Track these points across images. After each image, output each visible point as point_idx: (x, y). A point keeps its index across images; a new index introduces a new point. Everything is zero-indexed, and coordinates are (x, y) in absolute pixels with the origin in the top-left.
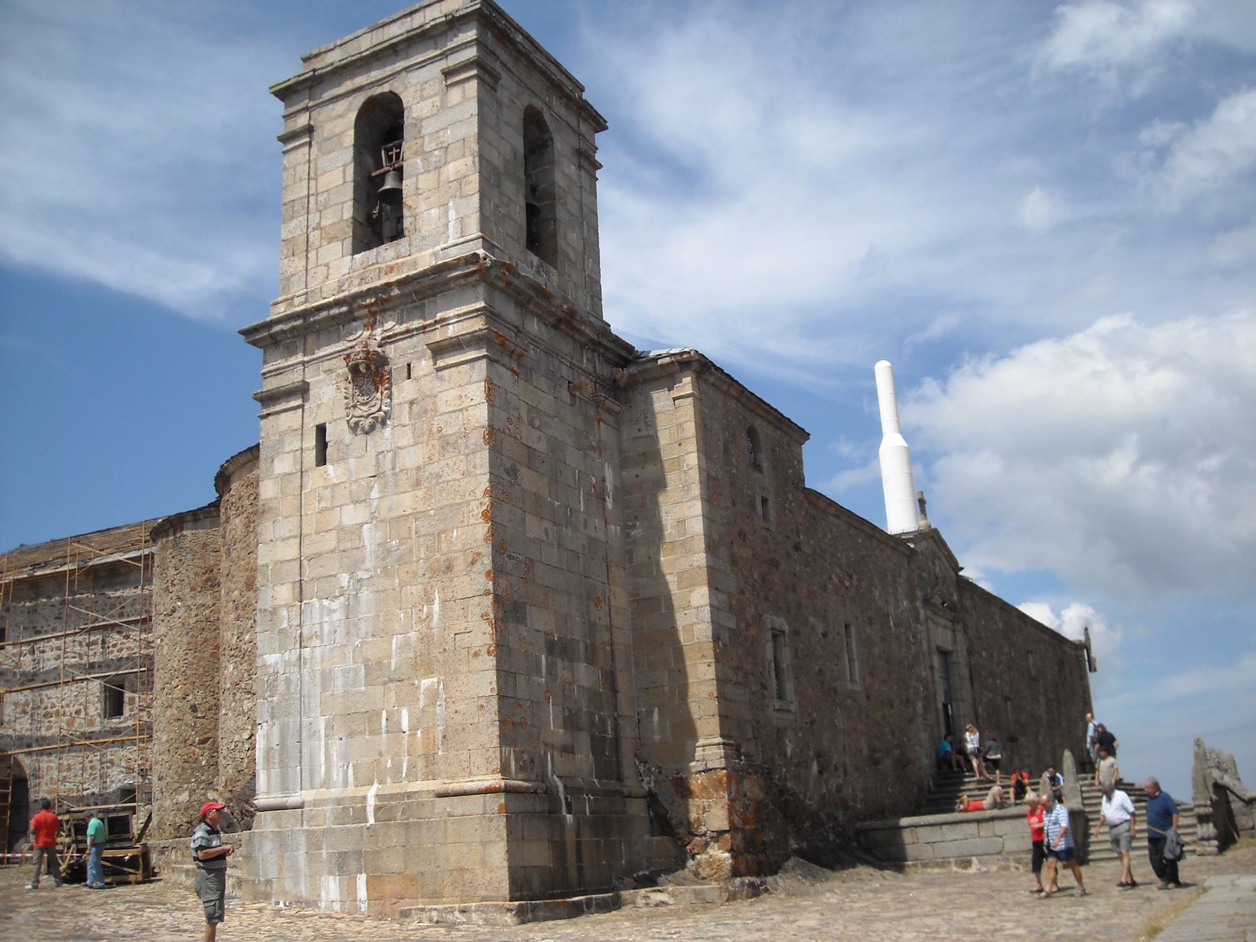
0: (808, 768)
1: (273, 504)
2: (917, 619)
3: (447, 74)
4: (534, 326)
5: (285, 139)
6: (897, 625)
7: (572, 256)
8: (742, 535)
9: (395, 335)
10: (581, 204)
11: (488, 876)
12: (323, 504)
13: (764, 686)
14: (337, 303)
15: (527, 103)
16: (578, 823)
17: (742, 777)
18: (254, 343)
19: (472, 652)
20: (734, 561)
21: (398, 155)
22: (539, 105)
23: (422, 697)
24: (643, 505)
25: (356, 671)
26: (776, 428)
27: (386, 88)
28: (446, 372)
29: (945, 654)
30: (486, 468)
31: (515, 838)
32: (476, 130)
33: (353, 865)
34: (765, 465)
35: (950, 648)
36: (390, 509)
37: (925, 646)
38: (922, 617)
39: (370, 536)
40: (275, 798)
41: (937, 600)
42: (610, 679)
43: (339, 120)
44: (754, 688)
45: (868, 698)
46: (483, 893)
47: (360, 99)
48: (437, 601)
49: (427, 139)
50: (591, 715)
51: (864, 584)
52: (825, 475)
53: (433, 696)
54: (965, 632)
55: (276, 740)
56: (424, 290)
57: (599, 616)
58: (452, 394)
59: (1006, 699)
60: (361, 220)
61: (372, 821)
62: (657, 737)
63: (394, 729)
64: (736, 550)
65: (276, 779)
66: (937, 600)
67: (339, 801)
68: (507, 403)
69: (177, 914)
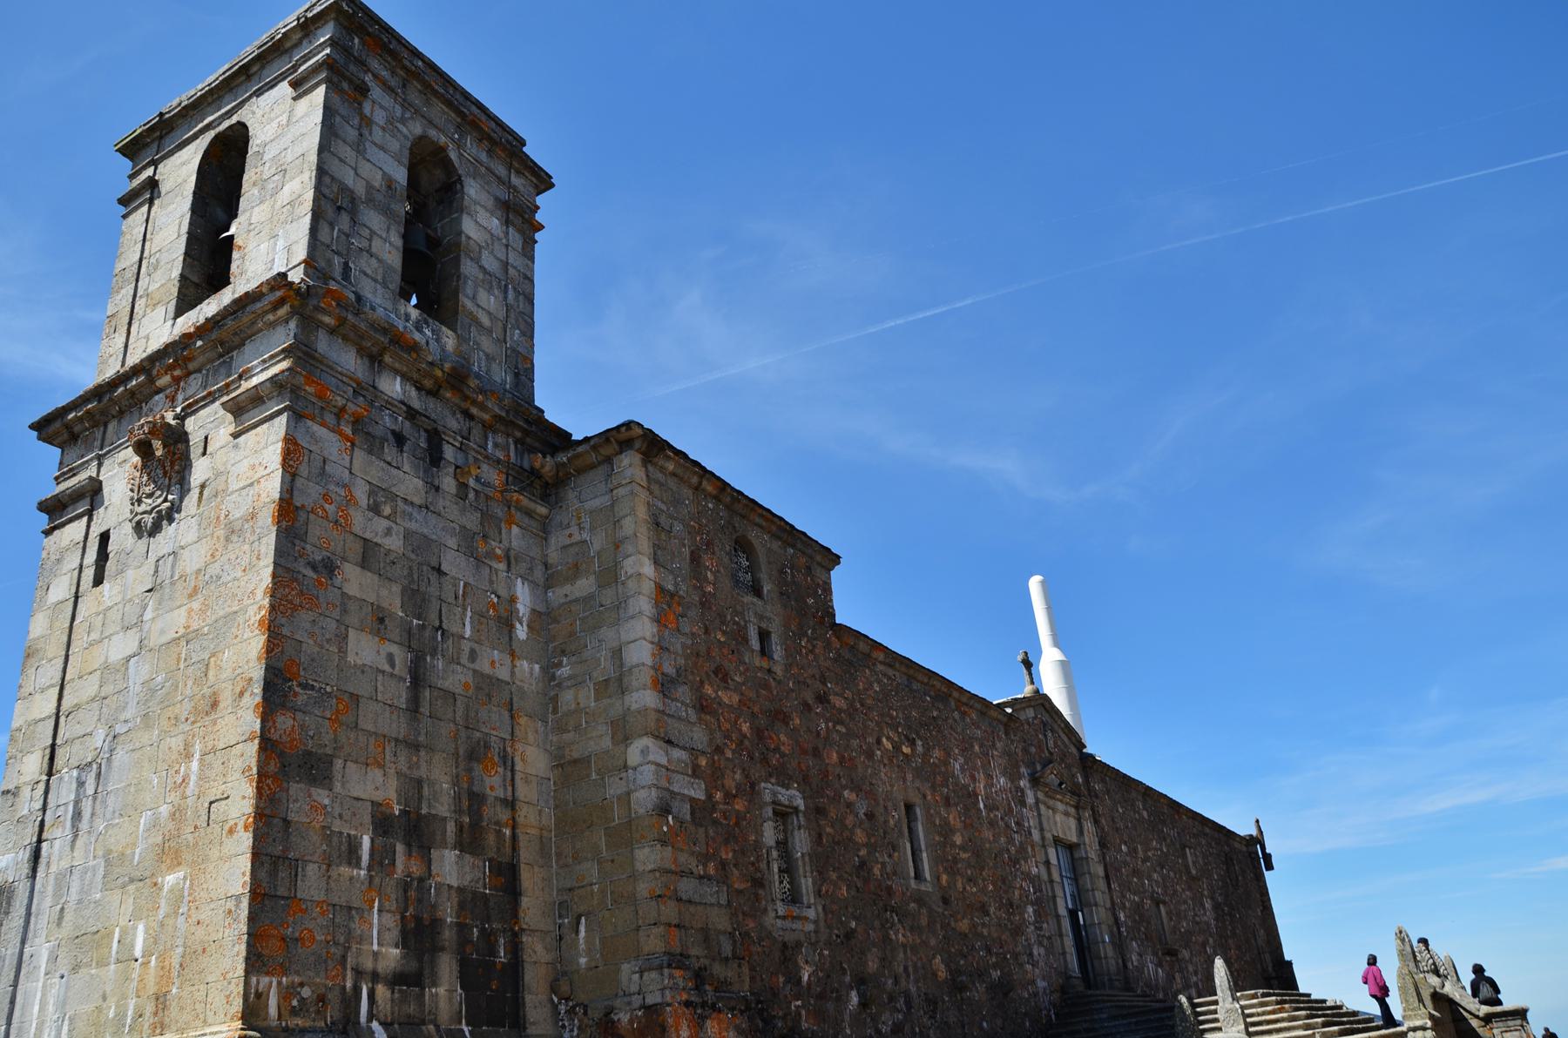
0: (841, 1000)
2: (1023, 803)
4: (393, 387)
5: (125, 201)
6: (989, 808)
9: (197, 402)
17: (703, 1018)
19: (227, 827)
23: (163, 903)
26: (787, 544)
27: (234, 119)
34: (767, 588)
35: (1074, 839)
37: (1036, 835)
38: (1030, 800)
42: (507, 875)
43: (181, 171)
48: (197, 756)
50: (461, 927)
51: (937, 753)
53: (177, 897)
54: (1096, 822)
57: (493, 783)
59: (1157, 903)
60: (195, 279)
62: (583, 960)
64: (709, 690)
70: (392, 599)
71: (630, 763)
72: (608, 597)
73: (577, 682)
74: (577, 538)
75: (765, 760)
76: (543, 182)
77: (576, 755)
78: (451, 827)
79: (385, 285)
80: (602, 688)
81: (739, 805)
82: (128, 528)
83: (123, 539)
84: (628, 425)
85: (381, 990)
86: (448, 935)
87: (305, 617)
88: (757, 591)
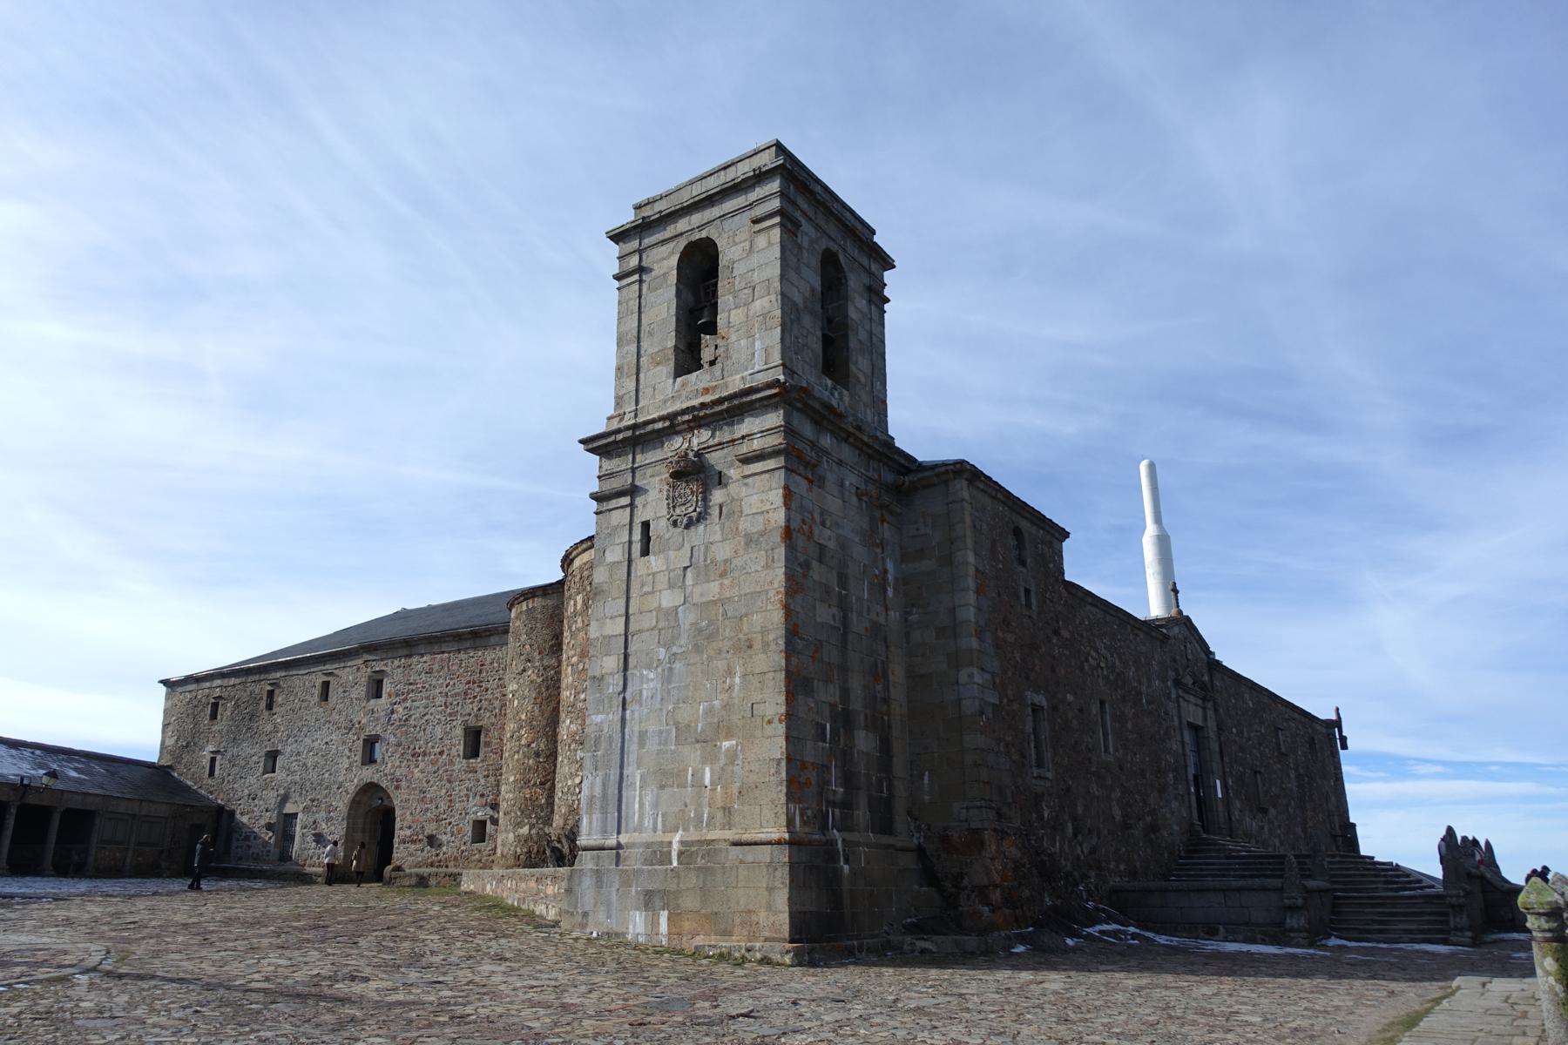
1: (605, 587)
2: (1169, 698)
3: (756, 221)
6: (1149, 703)
7: (863, 379)
10: (871, 334)
11: (772, 919)
12: (646, 589)
13: (1023, 756)
14: (662, 418)
16: (853, 872)
22: (835, 248)
27: (704, 234)
28: (750, 480)
29: (1194, 728)
30: (783, 563)
31: (796, 885)
32: (778, 272)
33: (657, 902)
35: (1200, 723)
36: (702, 595)
38: (1173, 696)
39: (687, 618)
41: (1189, 680)
43: (665, 261)
44: (1015, 757)
45: (1121, 768)
46: (767, 934)
47: (682, 243)
52: (1080, 567)
53: (732, 756)
54: (1216, 710)
55: (598, 790)
58: (754, 499)
61: (675, 864)
64: (1000, 634)
65: (596, 824)
66: (1189, 680)
67: (648, 845)
68: (801, 506)
69: (503, 941)
76: (888, 264)
81: (1015, 707)
82: (663, 523)
83: (659, 528)
84: (963, 462)
87: (799, 597)
88: (1023, 563)
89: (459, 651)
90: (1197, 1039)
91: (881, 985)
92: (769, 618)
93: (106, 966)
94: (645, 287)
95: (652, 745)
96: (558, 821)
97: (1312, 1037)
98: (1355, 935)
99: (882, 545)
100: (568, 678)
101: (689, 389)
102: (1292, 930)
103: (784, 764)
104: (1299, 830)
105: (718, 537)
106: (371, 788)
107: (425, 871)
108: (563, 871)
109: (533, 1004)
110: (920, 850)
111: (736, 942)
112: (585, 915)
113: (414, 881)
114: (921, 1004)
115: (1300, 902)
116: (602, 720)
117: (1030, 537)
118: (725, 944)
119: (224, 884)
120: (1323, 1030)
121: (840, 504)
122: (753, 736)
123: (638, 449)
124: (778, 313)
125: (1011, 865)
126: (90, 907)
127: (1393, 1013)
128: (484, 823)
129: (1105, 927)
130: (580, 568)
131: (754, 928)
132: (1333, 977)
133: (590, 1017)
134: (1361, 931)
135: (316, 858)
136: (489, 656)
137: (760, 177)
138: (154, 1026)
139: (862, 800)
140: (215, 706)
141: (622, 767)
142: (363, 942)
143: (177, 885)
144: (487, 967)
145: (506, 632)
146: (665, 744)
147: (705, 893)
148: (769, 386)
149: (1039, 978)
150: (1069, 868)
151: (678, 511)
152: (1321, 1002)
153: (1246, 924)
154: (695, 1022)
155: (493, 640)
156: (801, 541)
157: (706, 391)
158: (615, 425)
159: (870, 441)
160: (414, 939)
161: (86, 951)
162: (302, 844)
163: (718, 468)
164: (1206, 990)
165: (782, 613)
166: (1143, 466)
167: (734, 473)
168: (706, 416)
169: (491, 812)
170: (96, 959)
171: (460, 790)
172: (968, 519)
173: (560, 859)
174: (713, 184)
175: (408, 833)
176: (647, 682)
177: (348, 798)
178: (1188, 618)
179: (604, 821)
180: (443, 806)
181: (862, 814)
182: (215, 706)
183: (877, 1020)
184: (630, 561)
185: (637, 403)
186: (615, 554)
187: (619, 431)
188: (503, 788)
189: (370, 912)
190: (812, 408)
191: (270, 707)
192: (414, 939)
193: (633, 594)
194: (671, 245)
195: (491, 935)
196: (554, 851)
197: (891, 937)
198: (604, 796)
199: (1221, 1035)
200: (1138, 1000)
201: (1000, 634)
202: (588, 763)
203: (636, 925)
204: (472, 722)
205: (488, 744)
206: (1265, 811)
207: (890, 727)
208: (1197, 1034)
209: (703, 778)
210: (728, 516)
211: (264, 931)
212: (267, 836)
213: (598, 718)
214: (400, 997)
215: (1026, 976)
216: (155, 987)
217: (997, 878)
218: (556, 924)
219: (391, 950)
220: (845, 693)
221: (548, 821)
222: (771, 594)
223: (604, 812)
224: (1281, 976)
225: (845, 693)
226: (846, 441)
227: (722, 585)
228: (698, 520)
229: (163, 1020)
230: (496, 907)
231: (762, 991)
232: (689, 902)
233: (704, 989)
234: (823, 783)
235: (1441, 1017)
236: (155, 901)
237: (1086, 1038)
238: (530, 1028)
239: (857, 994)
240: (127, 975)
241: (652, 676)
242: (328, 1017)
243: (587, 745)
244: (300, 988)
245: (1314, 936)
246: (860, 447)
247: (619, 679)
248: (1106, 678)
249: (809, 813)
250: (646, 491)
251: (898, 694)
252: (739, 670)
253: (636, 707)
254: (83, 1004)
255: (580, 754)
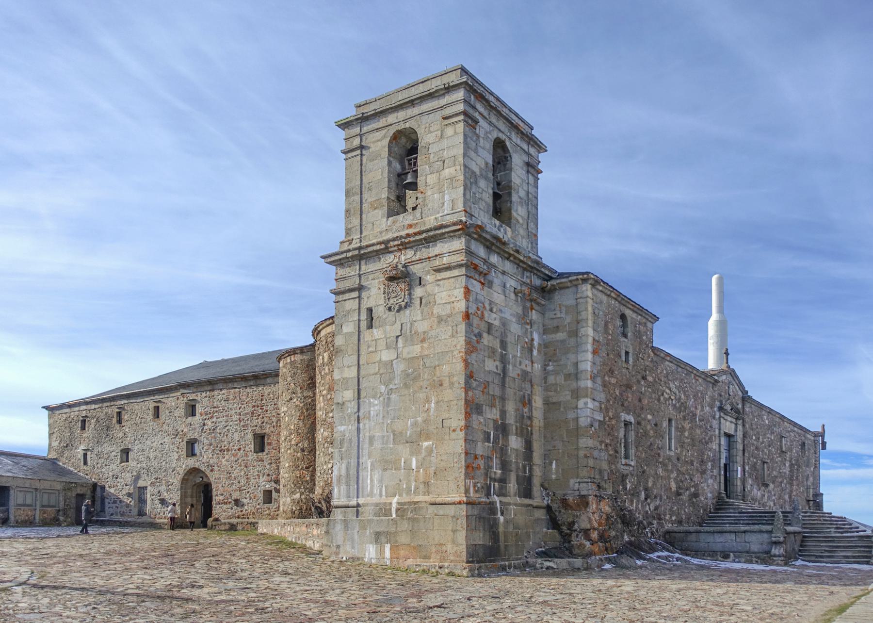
1: (343, 348)
2: (714, 418)
3: (445, 118)
6: (700, 420)
7: (521, 221)
8: (611, 371)
11: (455, 549)
12: (371, 349)
13: (616, 452)
15: (495, 136)
16: (507, 522)
18: (330, 263)
20: (605, 385)
21: (415, 163)
24: (555, 354)
25: (388, 437)
27: (407, 125)
28: (441, 283)
29: (729, 436)
30: (463, 334)
36: (408, 353)
38: (717, 416)
39: (399, 367)
40: (343, 501)
41: (728, 407)
43: (379, 143)
44: (611, 452)
45: (678, 459)
46: (452, 558)
47: (392, 130)
49: (432, 155)
52: (665, 339)
53: (430, 451)
54: (744, 425)
55: (343, 472)
56: (431, 237)
58: (444, 294)
61: (394, 516)
62: (554, 476)
63: (408, 468)
64: (607, 378)
66: (728, 407)
67: (377, 505)
68: (476, 300)
69: (286, 563)
70: (497, 345)
71: (579, 406)
72: (572, 342)
73: (556, 373)
74: (559, 315)
75: (622, 405)
76: (540, 147)
77: (554, 401)
78: (514, 428)
79: (487, 212)
80: (568, 377)
81: (613, 422)
82: (381, 309)
83: (380, 311)
85: (496, 484)
86: (513, 466)
87: (474, 355)
88: (625, 335)
89: (246, 387)
90: (713, 619)
91: (522, 588)
92: (453, 368)
93: (33, 581)
94: (364, 158)
95: (378, 445)
96: (318, 490)
97: (781, 619)
98: (813, 559)
99: (531, 324)
100: (320, 404)
101: (398, 225)
102: (775, 556)
103: (463, 456)
104: (786, 497)
105: (419, 317)
106: (194, 471)
107: (234, 521)
108: (324, 520)
109: (307, 601)
110: (548, 508)
111: (433, 562)
112: (338, 547)
113: (227, 527)
114: (546, 599)
115: (782, 539)
116: (344, 429)
117: (628, 318)
118: (425, 564)
119: (104, 530)
120: (788, 614)
121: (503, 298)
122: (443, 439)
123: (363, 262)
124: (462, 178)
125: (604, 516)
126: (16, 545)
127: (831, 604)
128: (271, 491)
129: (660, 554)
130: (326, 337)
131: (444, 554)
132: (797, 583)
133: (343, 608)
134: (817, 557)
135: (164, 515)
136: (267, 390)
137: (449, 89)
138: (68, 617)
139: (513, 477)
140: (84, 422)
141: (358, 458)
142: (197, 564)
143: (72, 531)
144: (277, 579)
145: (277, 375)
146: (386, 444)
147: (413, 533)
148: (454, 224)
149: (619, 584)
150: (641, 518)
151: (392, 301)
152: (788, 598)
153: (747, 552)
154: (408, 611)
155: (269, 380)
156: (475, 321)
157: (410, 226)
158: (346, 247)
159: (525, 260)
160: (230, 562)
161: (18, 572)
162: (152, 506)
163: (419, 275)
164: (719, 590)
165: (462, 364)
166: (714, 279)
167: (429, 278)
168: (409, 242)
169: (275, 485)
170: (25, 577)
171: (253, 472)
172: (590, 309)
173: (321, 513)
174: (415, 92)
175: (221, 498)
176: (374, 407)
177: (180, 477)
178: (733, 370)
179: (348, 490)
180: (243, 482)
181: (512, 486)
182: (84, 422)
183: (519, 609)
184: (359, 332)
185: (361, 234)
186: (349, 328)
187: (349, 251)
188: (282, 471)
189: (200, 546)
190: (485, 238)
191: (119, 422)
192: (230, 562)
193: (363, 352)
194: (384, 132)
195: (279, 559)
196: (317, 509)
197: (529, 560)
198: (348, 475)
199: (727, 617)
200: (678, 597)
201: (607, 378)
202: (336, 455)
203: (370, 552)
204: (258, 430)
205: (270, 444)
206: (767, 485)
207: (532, 434)
208: (713, 617)
209: (411, 464)
210: (426, 305)
211: (132, 558)
212: (127, 500)
213: (342, 428)
214: (224, 597)
215: (611, 582)
216: (66, 593)
217: (596, 525)
218: (320, 552)
219: (216, 569)
220: (503, 413)
221: (312, 490)
222: (456, 353)
223: (348, 484)
224: (766, 582)
225: (503, 413)
226: (508, 259)
227: (422, 347)
228: (405, 307)
229: (73, 614)
230: (281, 542)
231: (449, 592)
232: (403, 539)
233: (413, 591)
234: (488, 468)
235: (860, 607)
236: (59, 541)
237: (646, 619)
238: (306, 615)
239: (507, 593)
240: (47, 586)
241: (376, 402)
242: (179, 610)
243: (335, 444)
244: (159, 593)
245: (788, 559)
246: (518, 263)
247: (354, 404)
248: (674, 406)
249: (479, 485)
250: (369, 289)
251: (538, 414)
252: (434, 399)
253: (366, 421)
254: (20, 605)
255: (331, 450)
